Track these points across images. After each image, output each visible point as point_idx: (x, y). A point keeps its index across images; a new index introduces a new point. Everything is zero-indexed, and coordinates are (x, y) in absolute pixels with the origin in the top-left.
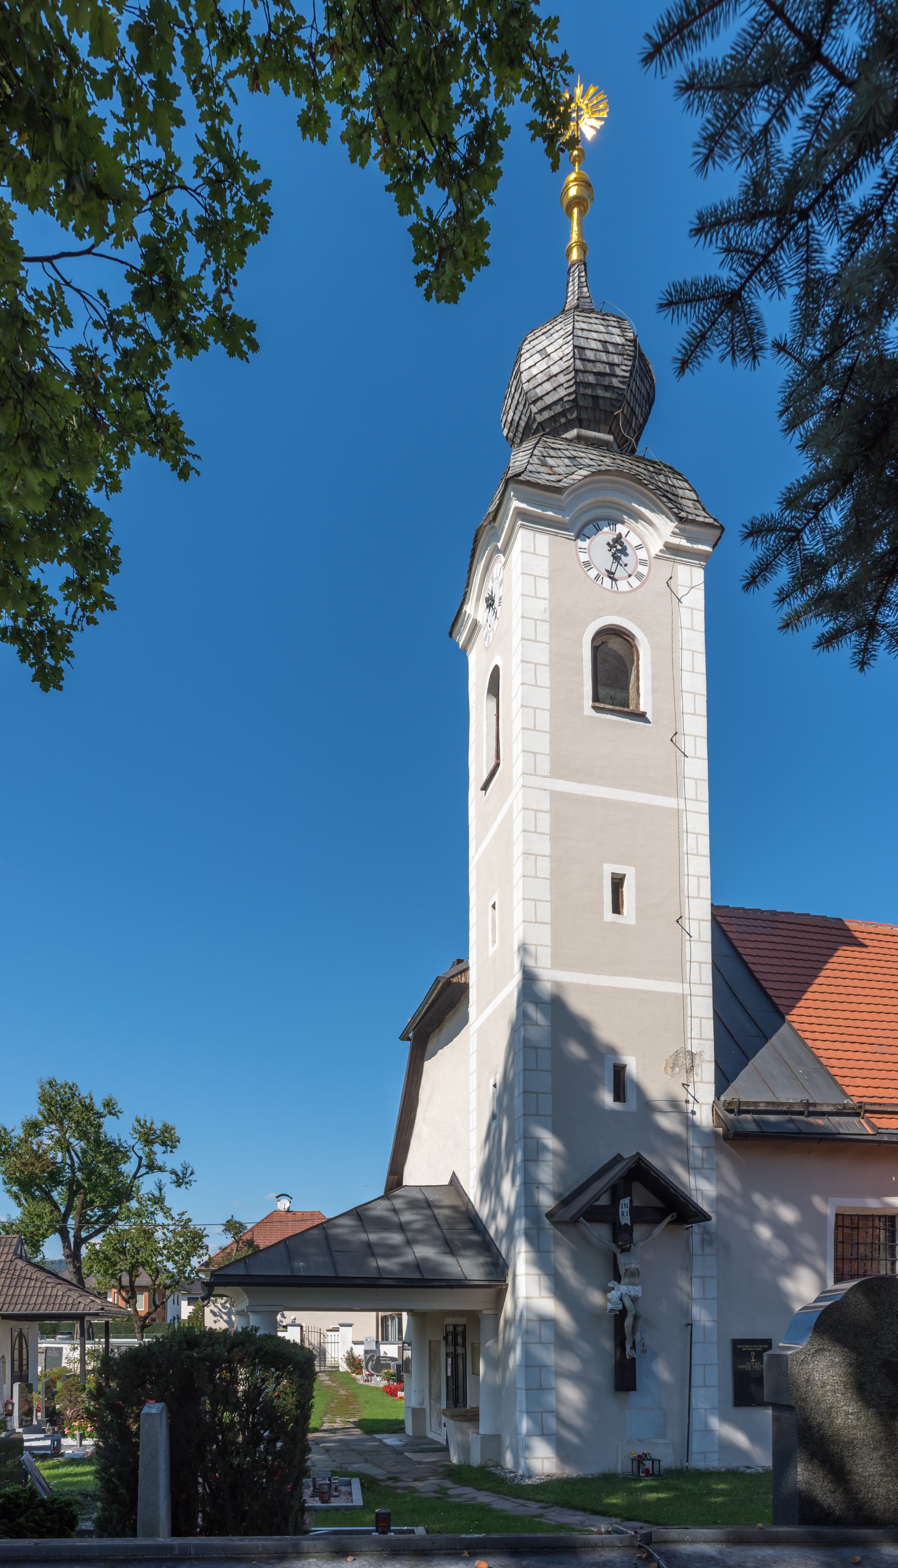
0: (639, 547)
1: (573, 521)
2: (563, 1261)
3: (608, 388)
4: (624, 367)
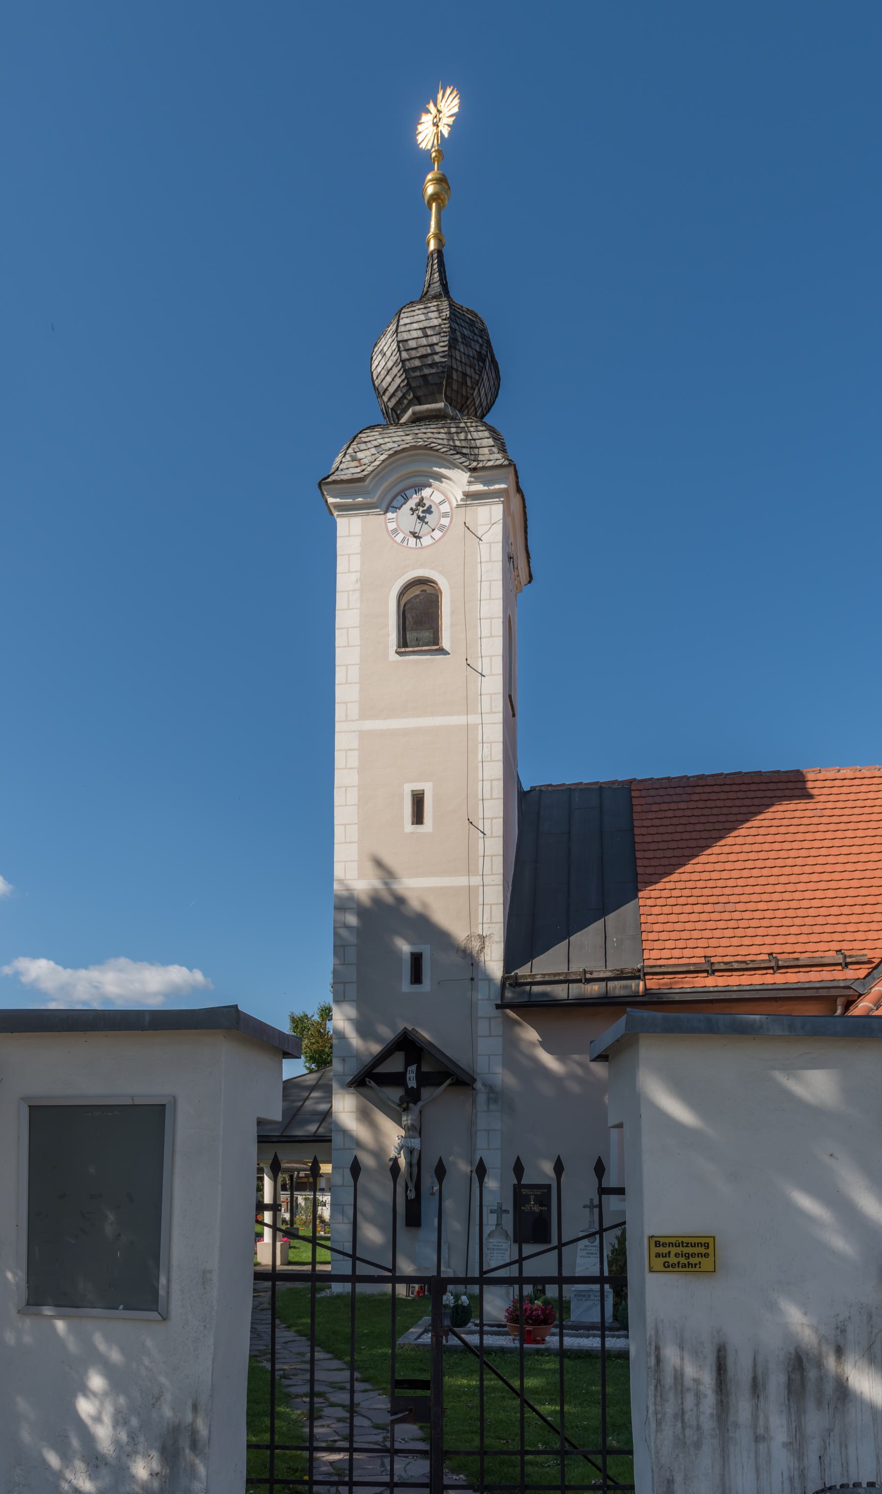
0: (441, 503)
1: (382, 498)
3: (433, 365)
4: (442, 344)
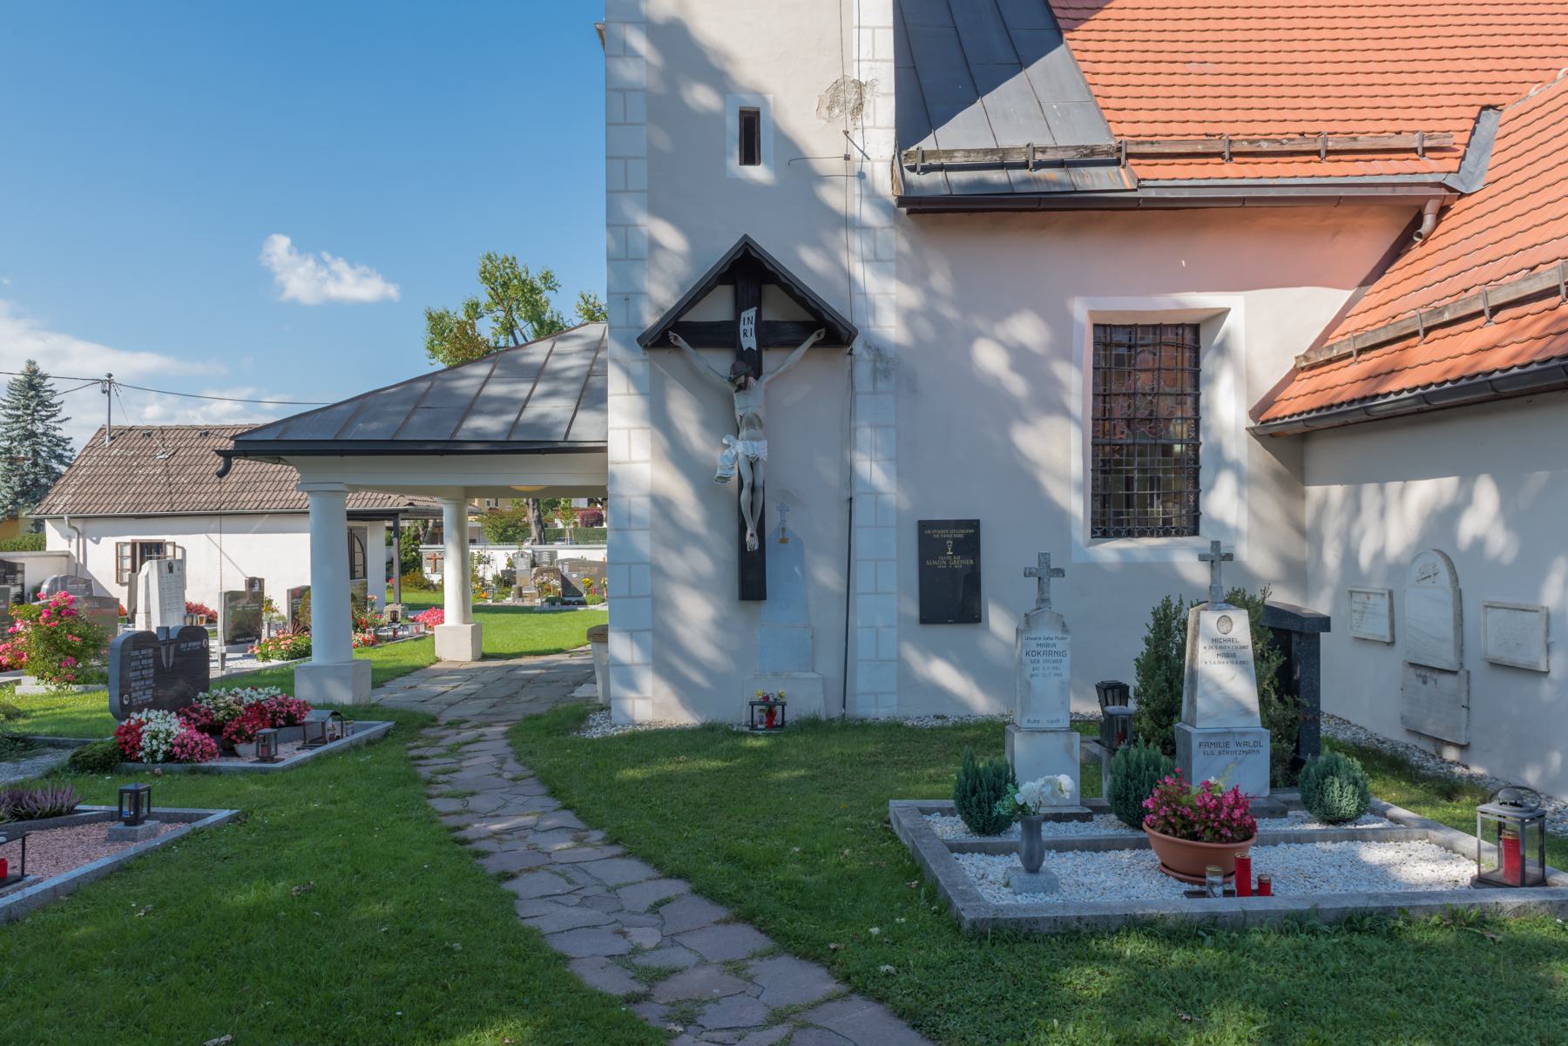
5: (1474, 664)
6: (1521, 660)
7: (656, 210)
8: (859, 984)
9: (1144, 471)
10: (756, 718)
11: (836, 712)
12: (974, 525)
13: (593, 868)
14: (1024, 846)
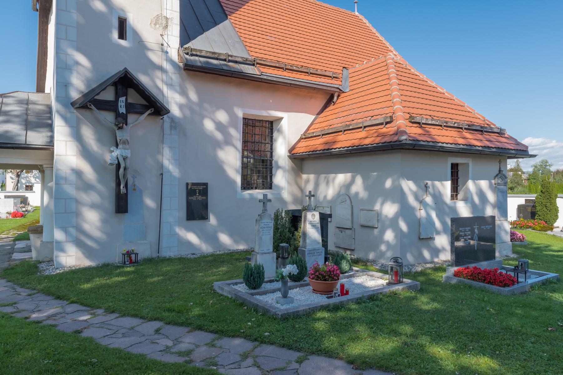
2: (88, 133)
5: (356, 226)
6: (370, 224)
7: (79, 50)
8: (260, 340)
9: (258, 169)
10: (126, 260)
11: (155, 255)
12: (206, 184)
13: (113, 322)
14: (282, 290)
